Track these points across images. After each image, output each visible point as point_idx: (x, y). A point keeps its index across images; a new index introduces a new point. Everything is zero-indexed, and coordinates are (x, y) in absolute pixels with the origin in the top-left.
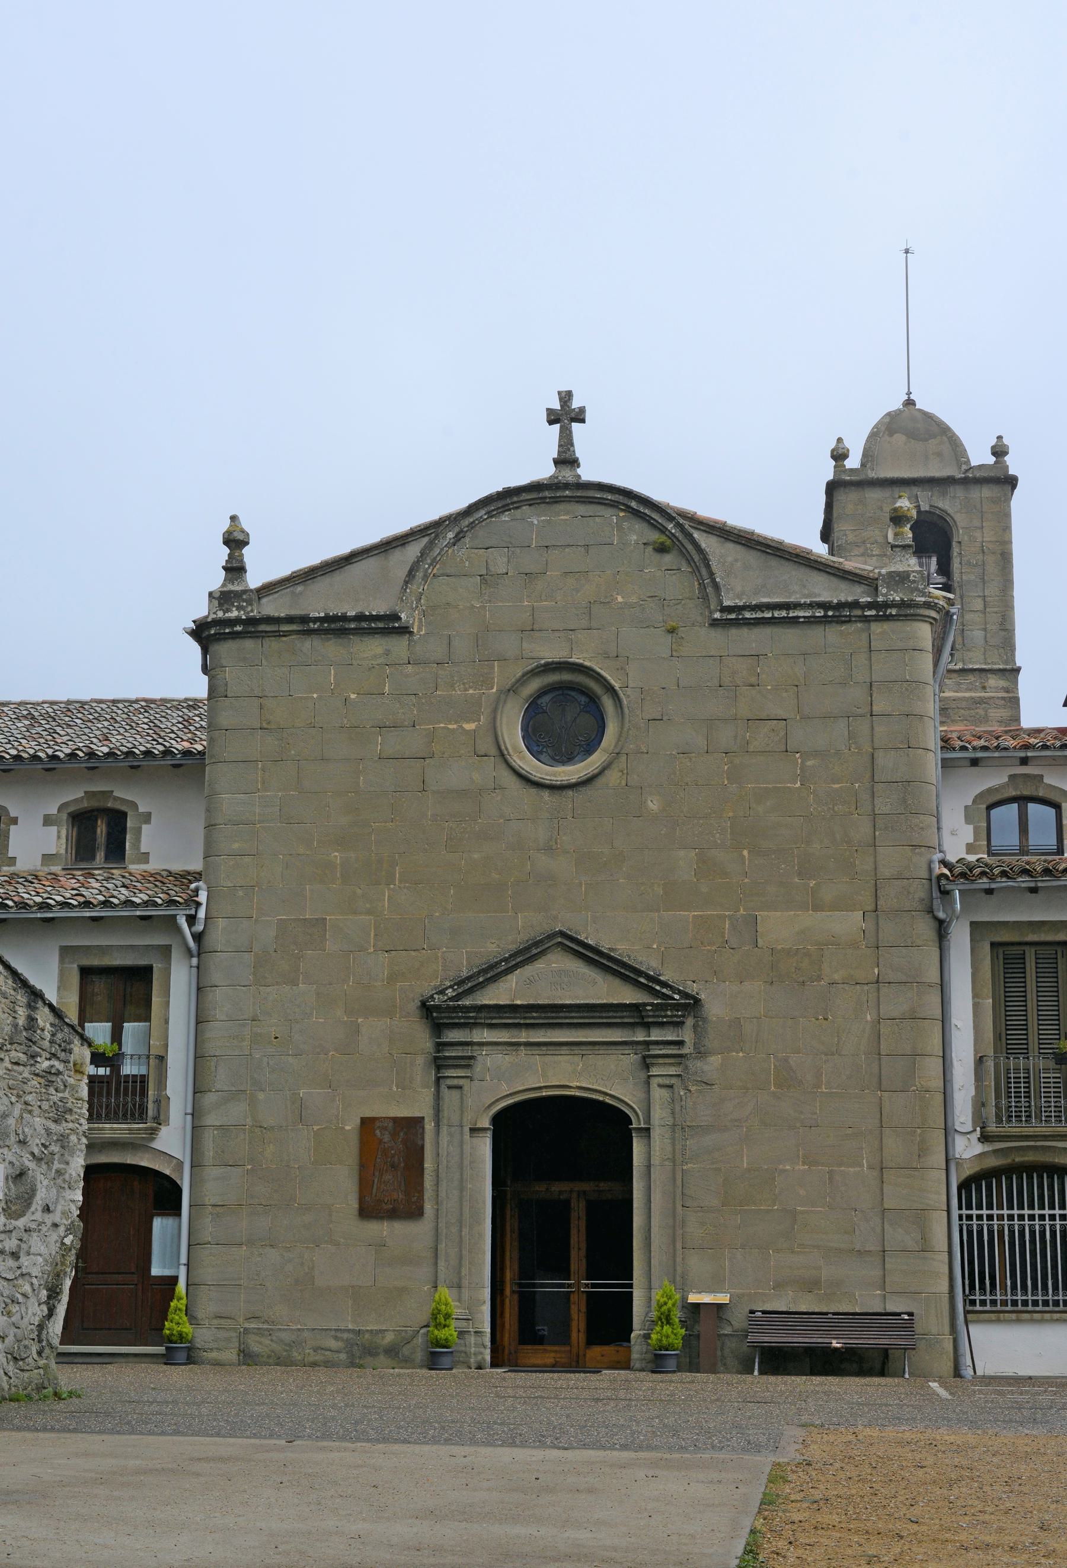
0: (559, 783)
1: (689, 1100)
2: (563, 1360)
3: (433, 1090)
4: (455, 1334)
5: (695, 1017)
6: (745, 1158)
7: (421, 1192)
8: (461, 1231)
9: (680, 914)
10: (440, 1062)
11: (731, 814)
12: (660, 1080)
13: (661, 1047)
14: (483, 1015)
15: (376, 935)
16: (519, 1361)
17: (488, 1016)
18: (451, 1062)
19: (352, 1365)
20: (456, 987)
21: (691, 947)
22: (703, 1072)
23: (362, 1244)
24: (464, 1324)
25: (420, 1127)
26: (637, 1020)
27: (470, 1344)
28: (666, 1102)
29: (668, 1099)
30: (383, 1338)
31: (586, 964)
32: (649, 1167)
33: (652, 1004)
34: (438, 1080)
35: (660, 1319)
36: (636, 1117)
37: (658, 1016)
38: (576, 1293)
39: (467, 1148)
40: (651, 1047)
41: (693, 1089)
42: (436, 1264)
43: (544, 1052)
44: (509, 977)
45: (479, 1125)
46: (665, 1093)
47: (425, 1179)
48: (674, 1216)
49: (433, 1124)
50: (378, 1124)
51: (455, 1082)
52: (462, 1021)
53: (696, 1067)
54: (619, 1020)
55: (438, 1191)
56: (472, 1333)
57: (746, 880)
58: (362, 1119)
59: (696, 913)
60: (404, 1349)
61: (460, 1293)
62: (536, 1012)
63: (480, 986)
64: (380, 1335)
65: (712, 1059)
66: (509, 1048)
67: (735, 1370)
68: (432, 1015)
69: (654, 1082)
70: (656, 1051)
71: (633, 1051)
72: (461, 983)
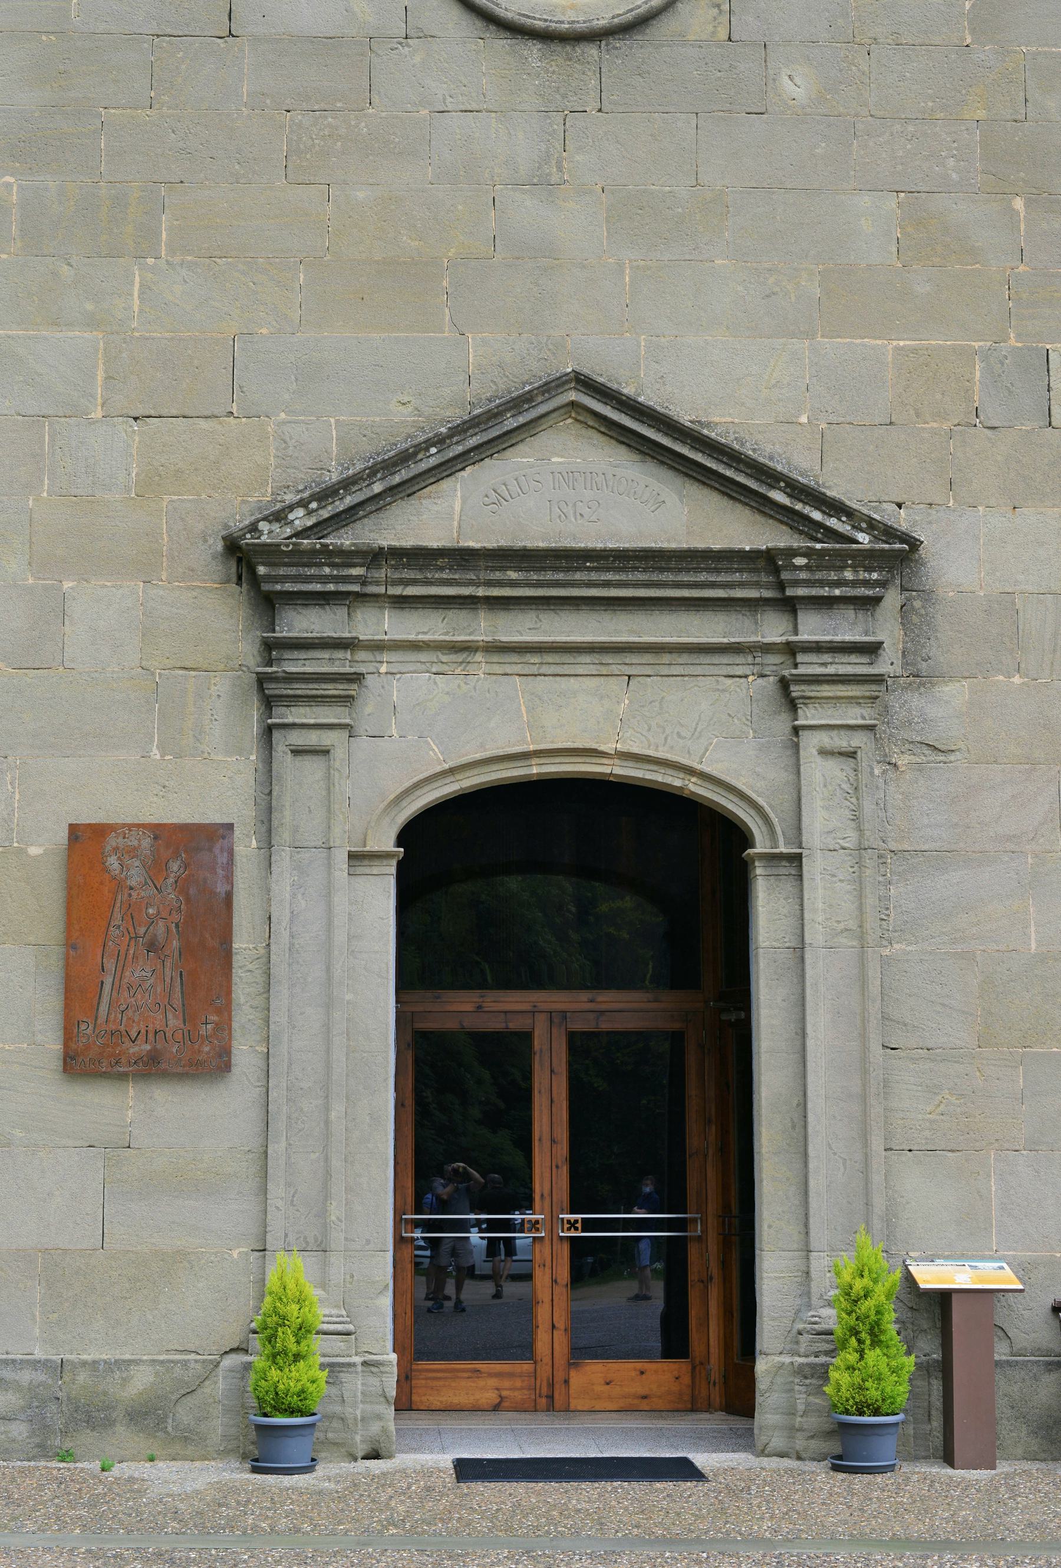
0: (567, 26)
1: (892, 788)
2: (518, 1395)
3: (253, 757)
4: (323, 1375)
5: (904, 589)
6: (1033, 929)
7: (225, 1008)
8: (327, 1109)
9: (864, 345)
10: (272, 689)
11: (981, 114)
12: (824, 739)
13: (826, 658)
14: (381, 574)
15: (108, 378)
16: (415, 1398)
17: (397, 576)
18: (301, 689)
19: (44, 1451)
20: (314, 505)
21: (891, 423)
22: (925, 721)
23: (70, 1143)
24: (337, 1344)
25: (222, 850)
26: (767, 594)
27: (355, 1396)
28: (838, 792)
29: (844, 786)
30: (125, 1380)
31: (637, 457)
32: (800, 949)
33: (808, 553)
34: (269, 731)
35: (855, 1332)
36: (764, 828)
37: (822, 583)
38: (547, 1242)
39: (341, 901)
40: (800, 658)
41: (902, 761)
42: (264, 1190)
43: (534, 670)
44: (446, 485)
45: (372, 846)
46: (836, 771)
47: (235, 979)
48: (865, 1069)
49: (254, 844)
50: (112, 841)
51: (313, 738)
52: (331, 587)
53: (909, 711)
54: (720, 593)
55: (268, 1010)
56: (360, 1368)
57: (1022, 268)
58: (73, 829)
59: (902, 343)
60: (179, 1409)
61: (325, 1265)
62: (518, 569)
63: (376, 503)
64: (117, 1374)
65: (948, 689)
66: (444, 658)
67: (1020, 1451)
68: (252, 571)
69: (810, 742)
70: (810, 665)
71: (756, 669)
72: (326, 495)
